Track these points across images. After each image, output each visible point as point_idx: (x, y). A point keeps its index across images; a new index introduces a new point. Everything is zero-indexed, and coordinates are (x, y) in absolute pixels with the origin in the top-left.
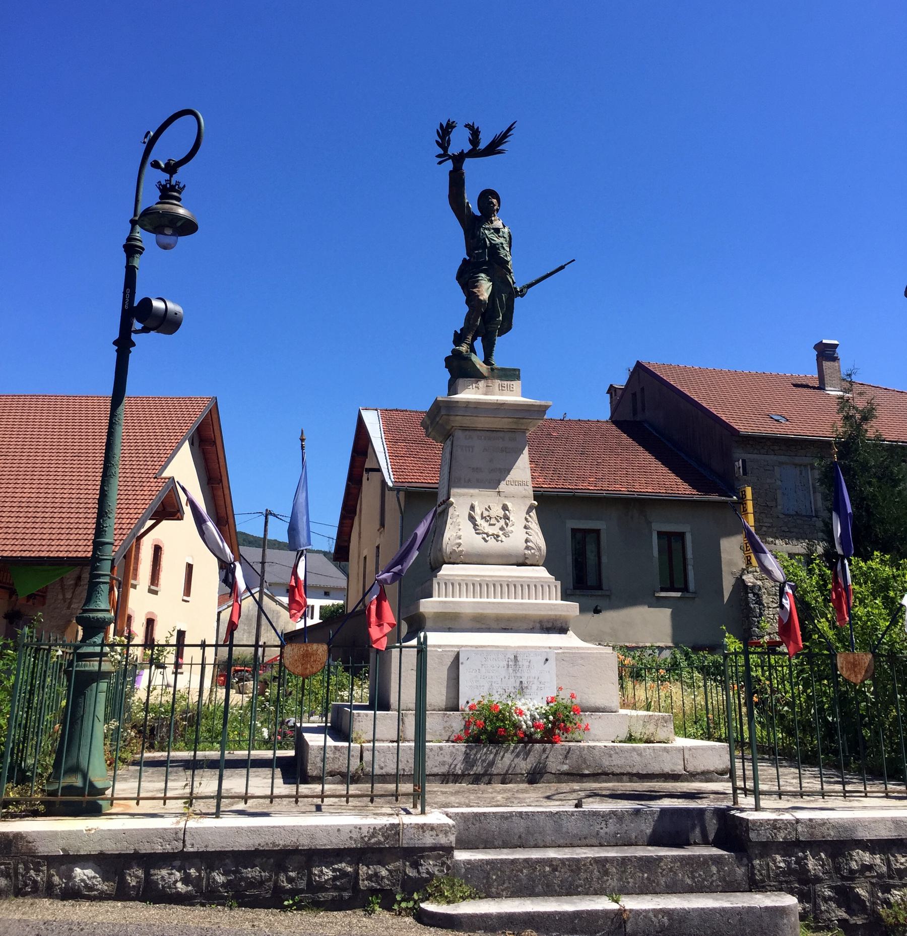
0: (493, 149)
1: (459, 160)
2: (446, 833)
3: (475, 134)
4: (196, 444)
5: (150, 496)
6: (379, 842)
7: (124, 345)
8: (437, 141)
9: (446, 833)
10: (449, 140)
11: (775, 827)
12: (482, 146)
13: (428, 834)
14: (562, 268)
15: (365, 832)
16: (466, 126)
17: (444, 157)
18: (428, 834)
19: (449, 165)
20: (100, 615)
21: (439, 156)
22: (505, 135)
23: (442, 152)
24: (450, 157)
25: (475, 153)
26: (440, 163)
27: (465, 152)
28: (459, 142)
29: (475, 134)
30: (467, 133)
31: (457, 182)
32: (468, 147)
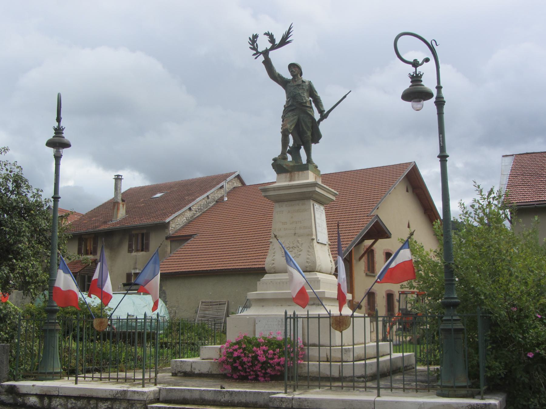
0: (284, 41)
1: (266, 53)
2: (143, 395)
3: (272, 39)
4: (410, 190)
5: (366, 224)
6: (119, 396)
7: (329, 112)
8: (250, 48)
9: (143, 395)
10: (257, 45)
11: (281, 401)
12: (277, 42)
13: (136, 395)
14: (345, 97)
15: (114, 392)
16: (266, 34)
17: (257, 54)
18: (136, 395)
19: (262, 58)
20: (55, 308)
21: (254, 55)
22: (289, 33)
23: (255, 52)
24: (261, 53)
25: (274, 47)
26: (256, 58)
27: (268, 48)
28: (263, 44)
29: (271, 38)
30: (267, 38)
31: (268, 63)
32: (269, 45)
